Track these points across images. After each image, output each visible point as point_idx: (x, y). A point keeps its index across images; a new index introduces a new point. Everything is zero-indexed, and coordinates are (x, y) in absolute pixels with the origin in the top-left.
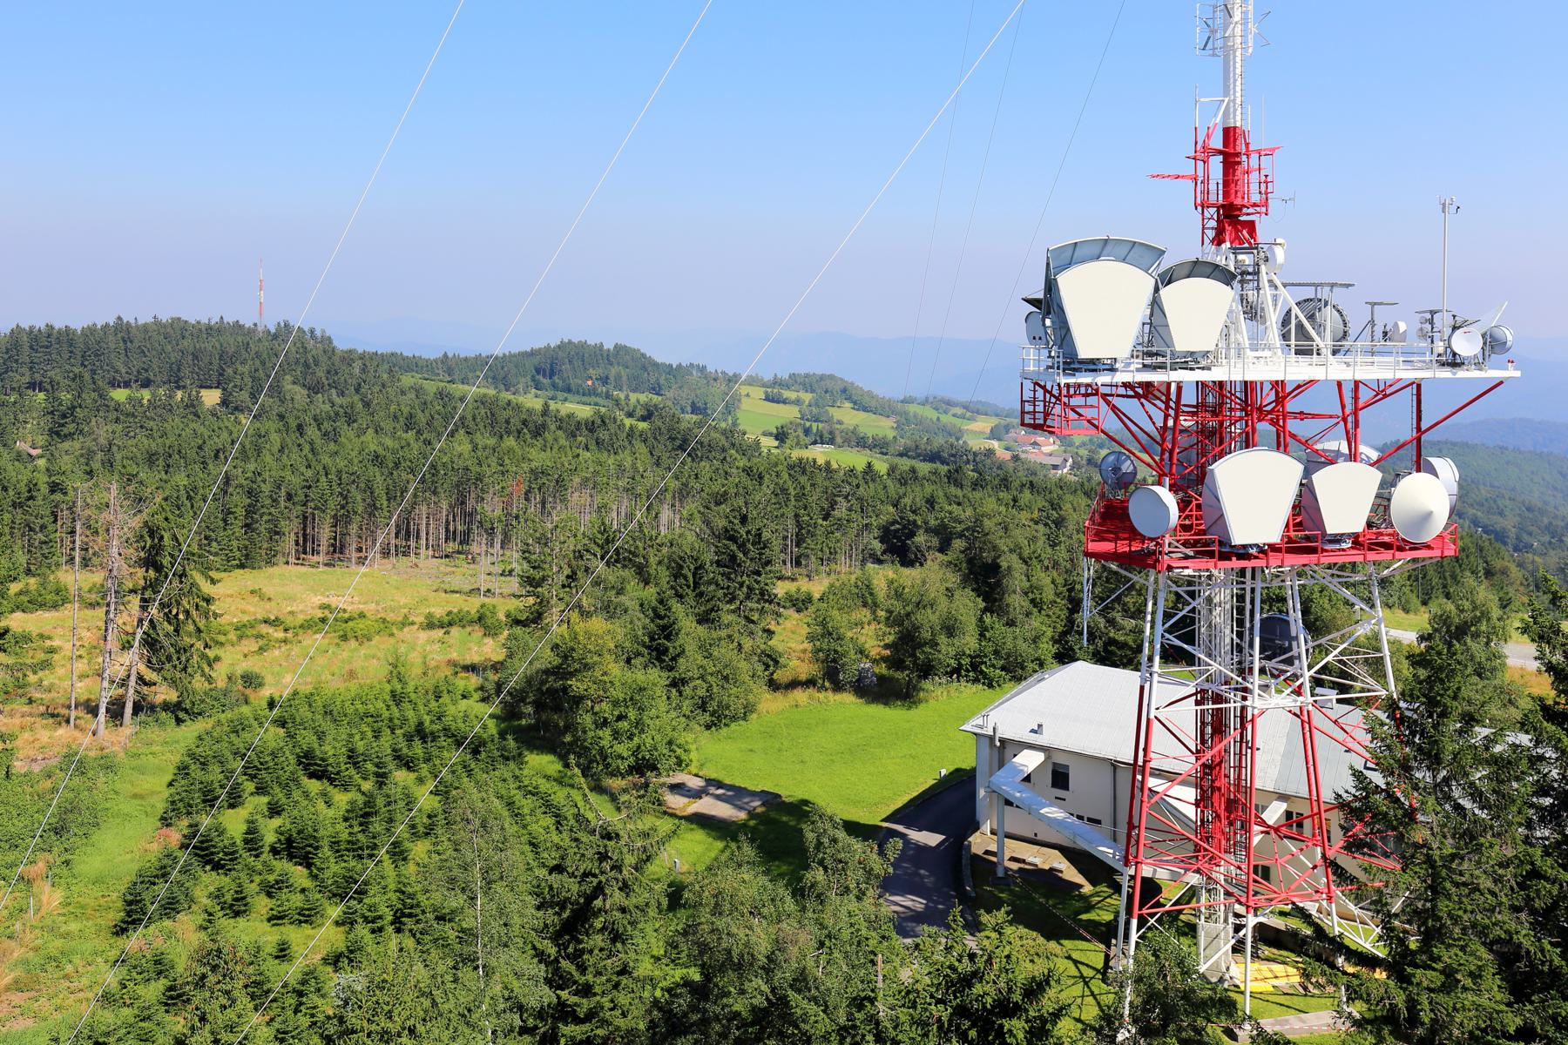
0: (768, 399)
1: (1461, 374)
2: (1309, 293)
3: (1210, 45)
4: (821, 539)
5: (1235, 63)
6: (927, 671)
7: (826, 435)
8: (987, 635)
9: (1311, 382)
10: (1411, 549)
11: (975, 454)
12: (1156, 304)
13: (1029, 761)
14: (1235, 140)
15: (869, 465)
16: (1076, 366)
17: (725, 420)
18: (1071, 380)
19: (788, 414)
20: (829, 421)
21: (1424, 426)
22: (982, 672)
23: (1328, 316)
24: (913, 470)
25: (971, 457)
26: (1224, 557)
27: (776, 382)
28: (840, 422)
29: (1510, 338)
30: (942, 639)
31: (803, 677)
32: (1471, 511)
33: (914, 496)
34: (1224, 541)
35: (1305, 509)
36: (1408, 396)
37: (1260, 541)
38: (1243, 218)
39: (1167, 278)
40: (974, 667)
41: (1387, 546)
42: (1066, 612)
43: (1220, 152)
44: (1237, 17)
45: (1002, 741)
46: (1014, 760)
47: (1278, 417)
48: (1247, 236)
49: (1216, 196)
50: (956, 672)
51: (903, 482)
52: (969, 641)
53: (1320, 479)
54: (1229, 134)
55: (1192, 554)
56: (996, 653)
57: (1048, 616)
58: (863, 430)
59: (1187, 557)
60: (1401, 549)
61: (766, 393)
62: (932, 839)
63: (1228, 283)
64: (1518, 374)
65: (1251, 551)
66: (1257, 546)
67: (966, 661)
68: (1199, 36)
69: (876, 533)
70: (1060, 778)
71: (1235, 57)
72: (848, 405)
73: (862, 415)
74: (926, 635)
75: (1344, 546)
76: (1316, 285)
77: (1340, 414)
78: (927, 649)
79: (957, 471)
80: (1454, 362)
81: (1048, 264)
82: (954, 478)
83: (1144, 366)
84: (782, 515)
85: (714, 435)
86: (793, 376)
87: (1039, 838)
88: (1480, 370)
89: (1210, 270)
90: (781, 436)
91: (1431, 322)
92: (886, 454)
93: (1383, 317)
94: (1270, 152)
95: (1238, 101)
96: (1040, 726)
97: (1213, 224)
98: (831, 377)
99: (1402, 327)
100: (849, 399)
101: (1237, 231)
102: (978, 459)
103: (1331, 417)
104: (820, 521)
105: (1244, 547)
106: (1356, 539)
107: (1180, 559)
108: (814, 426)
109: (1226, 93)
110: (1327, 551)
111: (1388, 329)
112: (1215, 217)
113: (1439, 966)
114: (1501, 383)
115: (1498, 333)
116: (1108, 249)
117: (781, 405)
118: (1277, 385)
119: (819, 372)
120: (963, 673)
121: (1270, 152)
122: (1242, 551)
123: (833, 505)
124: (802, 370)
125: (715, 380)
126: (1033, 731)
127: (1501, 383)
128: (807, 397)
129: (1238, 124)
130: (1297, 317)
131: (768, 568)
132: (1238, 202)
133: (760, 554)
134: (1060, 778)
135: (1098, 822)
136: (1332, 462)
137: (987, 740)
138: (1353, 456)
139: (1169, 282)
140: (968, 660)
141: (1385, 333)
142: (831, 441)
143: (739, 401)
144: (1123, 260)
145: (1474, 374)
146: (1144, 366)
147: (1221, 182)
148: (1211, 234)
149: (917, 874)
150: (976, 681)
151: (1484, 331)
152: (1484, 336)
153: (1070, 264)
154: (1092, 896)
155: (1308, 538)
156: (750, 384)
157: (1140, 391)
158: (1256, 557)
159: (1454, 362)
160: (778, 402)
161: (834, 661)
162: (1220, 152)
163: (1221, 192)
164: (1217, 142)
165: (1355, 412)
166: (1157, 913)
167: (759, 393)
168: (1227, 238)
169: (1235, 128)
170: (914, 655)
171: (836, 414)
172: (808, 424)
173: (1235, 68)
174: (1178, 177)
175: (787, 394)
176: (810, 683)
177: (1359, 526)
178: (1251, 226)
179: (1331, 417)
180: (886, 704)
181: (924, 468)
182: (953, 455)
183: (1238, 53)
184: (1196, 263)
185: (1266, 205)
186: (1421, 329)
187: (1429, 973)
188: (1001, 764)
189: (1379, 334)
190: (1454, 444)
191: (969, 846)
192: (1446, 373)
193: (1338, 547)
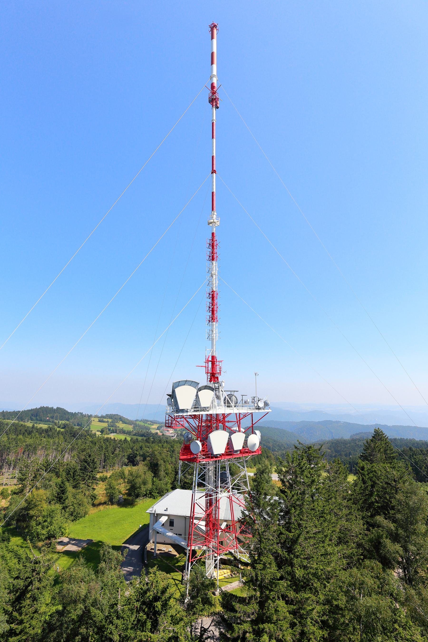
1: (260, 411)
2: (229, 393)
3: (209, 338)
7: (115, 431)
11: (153, 434)
12: (197, 396)
15: (126, 438)
16: (179, 411)
18: (178, 415)
19: (105, 425)
20: (116, 427)
22: (152, 495)
24: (137, 439)
27: (102, 417)
28: (119, 427)
30: (142, 486)
31: (103, 502)
32: (263, 442)
34: (212, 454)
35: (230, 444)
36: (250, 415)
37: (220, 453)
38: (216, 376)
39: (200, 390)
40: (150, 493)
41: (247, 452)
43: (211, 361)
44: (214, 332)
45: (157, 514)
47: (224, 422)
49: (210, 371)
51: (134, 443)
52: (149, 486)
53: (233, 437)
54: (213, 357)
55: (205, 457)
57: (170, 477)
58: (124, 429)
59: (203, 458)
60: (250, 453)
61: (99, 420)
62: (136, 547)
64: (271, 411)
66: (219, 454)
67: (148, 492)
72: (121, 422)
73: (125, 425)
74: (138, 485)
76: (231, 391)
78: (138, 489)
79: (148, 439)
80: (259, 408)
82: (147, 441)
90: (102, 431)
92: (130, 435)
94: (221, 361)
96: (167, 509)
97: (209, 377)
98: (117, 415)
99: (248, 401)
100: (122, 421)
103: (234, 422)
105: (216, 455)
107: (202, 459)
108: (111, 428)
115: (267, 402)
118: (223, 414)
120: (147, 495)
125: (85, 416)
126: (165, 510)
128: (110, 420)
132: (215, 372)
133: (93, 466)
135: (181, 535)
138: (239, 431)
139: (200, 391)
140: (149, 492)
141: (245, 402)
142: (116, 432)
144: (190, 385)
145: (263, 411)
146: (194, 411)
148: (209, 379)
150: (151, 497)
152: (264, 402)
153: (178, 386)
154: (179, 558)
155: (230, 452)
156: (94, 417)
158: (219, 457)
159: (259, 408)
162: (211, 361)
165: (240, 420)
167: (97, 420)
170: (134, 492)
171: (117, 424)
172: (110, 428)
175: (105, 420)
176: (105, 503)
178: (217, 378)
179: (234, 422)
180: (126, 507)
181: (140, 438)
182: (148, 435)
188: (156, 521)
189: (244, 402)
190: (259, 427)
192: (257, 411)
193: (237, 453)
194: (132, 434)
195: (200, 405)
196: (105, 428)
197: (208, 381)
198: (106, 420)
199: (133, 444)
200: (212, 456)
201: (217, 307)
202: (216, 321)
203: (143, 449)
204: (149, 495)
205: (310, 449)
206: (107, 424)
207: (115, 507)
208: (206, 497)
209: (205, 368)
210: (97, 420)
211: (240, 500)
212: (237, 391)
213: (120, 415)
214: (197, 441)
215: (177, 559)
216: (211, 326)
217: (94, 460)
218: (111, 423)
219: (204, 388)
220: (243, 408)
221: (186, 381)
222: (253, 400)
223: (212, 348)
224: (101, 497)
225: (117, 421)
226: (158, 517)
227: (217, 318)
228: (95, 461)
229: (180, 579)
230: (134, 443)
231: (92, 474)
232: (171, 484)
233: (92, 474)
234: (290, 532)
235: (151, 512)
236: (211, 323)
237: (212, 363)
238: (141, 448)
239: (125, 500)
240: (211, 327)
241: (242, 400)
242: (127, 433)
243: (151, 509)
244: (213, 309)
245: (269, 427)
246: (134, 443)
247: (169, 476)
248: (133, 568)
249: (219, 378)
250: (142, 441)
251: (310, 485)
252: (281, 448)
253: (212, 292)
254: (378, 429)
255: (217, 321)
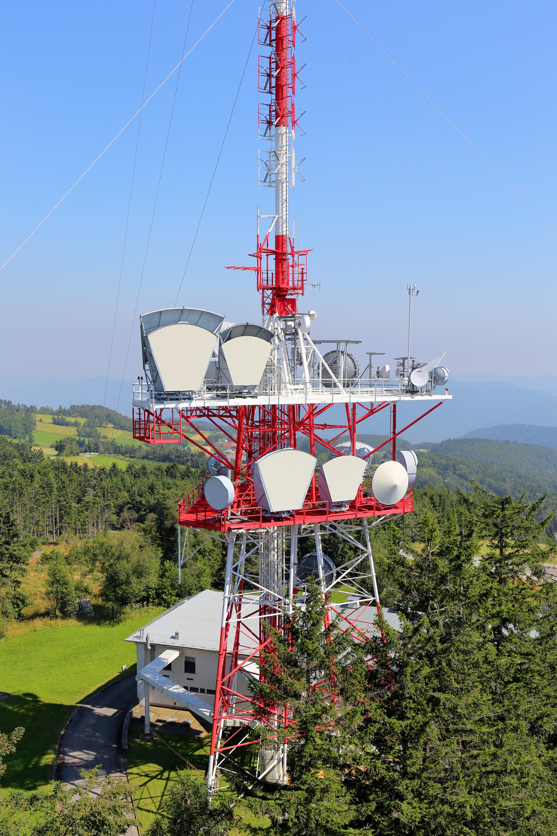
0: (56, 422)
1: (417, 398)
2: (333, 347)
3: (268, 180)
4: (74, 516)
5: (282, 191)
6: (124, 601)
7: (93, 446)
8: (167, 574)
9: (330, 405)
10: (385, 509)
11: (192, 455)
13: (170, 656)
14: (283, 244)
15: (114, 465)
16: (165, 396)
17: (24, 438)
18: (162, 406)
19: (70, 432)
20: (98, 436)
21: (397, 432)
22: (163, 599)
23: (342, 361)
24: (144, 468)
25: (189, 458)
26: (266, 520)
27: (61, 411)
28: (105, 437)
29: (447, 374)
30: (134, 579)
31: (43, 610)
32: (488, 480)
33: (142, 484)
34: (266, 511)
36: (388, 410)
37: (290, 509)
38: (288, 297)
39: (228, 336)
40: (158, 595)
41: (370, 508)
42: (221, 556)
43: (273, 252)
44: (283, 160)
45: (153, 646)
46: (160, 656)
47: (309, 428)
48: (290, 308)
50: (145, 600)
51: (136, 476)
52: (153, 580)
53: (327, 467)
54: (280, 240)
55: (246, 519)
56: (172, 586)
57: (209, 560)
58: (119, 442)
59: (243, 521)
60: (378, 509)
61: (54, 419)
62: (109, 712)
63: (268, 341)
64: (450, 397)
65: (283, 516)
66: (289, 512)
67: (152, 593)
68: (261, 173)
69: (113, 510)
70: (190, 666)
71: (282, 187)
72: (111, 425)
73: (120, 432)
74: (123, 577)
75: (344, 509)
76: (338, 342)
77: (348, 425)
78: (124, 587)
79: (172, 467)
80: (412, 390)
81: (141, 326)
82: (170, 473)
83: (217, 396)
84: (48, 502)
85: (8, 448)
86: (73, 407)
87: (178, 705)
88: (430, 395)
89: (256, 331)
90: (60, 448)
91: (403, 365)
92: (134, 457)
93: (377, 362)
94: (304, 253)
95: (284, 218)
96: (177, 634)
97: (269, 301)
98: (100, 407)
99: (388, 368)
100: (111, 421)
101: (285, 306)
102: (194, 459)
103: (341, 427)
104: (74, 504)
106: (352, 505)
107: (238, 523)
108: (87, 440)
109: (277, 212)
110: (332, 513)
111: (380, 370)
112: (271, 297)
113: (305, 787)
114: (441, 403)
115: (439, 371)
116: (185, 316)
117: (64, 427)
118: (312, 406)
119: (91, 404)
120: (151, 600)
121: (304, 253)
122: (278, 516)
123: (84, 493)
124: (79, 403)
125: (17, 410)
126: (173, 637)
127: (441, 403)
128: (82, 421)
129: (284, 234)
130: (323, 365)
131: (15, 539)
132: (284, 286)
133: (9, 530)
134: (190, 666)
136: (341, 455)
137: (143, 646)
139: (229, 339)
140: (154, 592)
141: (378, 372)
142: (96, 450)
143: (35, 424)
144: (196, 325)
145: (426, 398)
146: (217, 396)
147: (274, 272)
148: (267, 307)
149: (94, 735)
150: (159, 604)
151: (430, 370)
152: (431, 373)
153: (159, 326)
154: (206, 738)
155: (324, 506)
156: (42, 413)
157: (234, 413)
158: (287, 519)
159: (412, 390)
160: (62, 425)
161: (62, 598)
162: (273, 252)
163: (274, 279)
164: (272, 247)
165: (354, 425)
166: (241, 743)
167: (48, 419)
168: (277, 310)
169: (282, 236)
170: (114, 591)
171: (102, 431)
172: (82, 439)
173: (282, 195)
174: (246, 269)
175: (68, 419)
176: (47, 614)
177: (352, 496)
179: (341, 427)
180: (99, 624)
181: (151, 465)
182: (178, 457)
183: (284, 185)
184: (247, 326)
185: (302, 288)
186: (398, 370)
187: (300, 792)
188: (153, 658)
189: (374, 373)
190: (480, 440)
191: (132, 713)
192: (407, 398)
193: (339, 510)
194: (138, 454)
195: (230, 381)
196: (68, 439)
197: (266, 311)
198: (72, 420)
199: (133, 478)
200: (269, 515)
201: (294, 75)
202: (290, 124)
203: (155, 491)
204: (154, 599)
205: (507, 506)
206: (75, 429)
207: (73, 623)
208: (260, 615)
209: (254, 274)
210: (48, 419)
211: (351, 622)
212: (358, 342)
213: (107, 409)
214: (222, 478)
215: (200, 740)
216: (274, 139)
217: (8, 517)
218: (84, 426)
219: (241, 331)
220: (373, 389)
221: (182, 311)
222: (401, 368)
223: (277, 212)
224: (40, 601)
225: (101, 423)
226: (156, 652)
227: (293, 112)
228: (12, 519)
229: (142, 797)
230: (135, 476)
231: (7, 549)
232: (213, 575)
233: (7, 549)
234: (402, 717)
235: (138, 640)
236: (273, 127)
237: (276, 259)
238: (152, 488)
239: (97, 608)
240: (274, 143)
241: (370, 366)
242: (126, 453)
243: (138, 634)
244: (278, 78)
245: (507, 442)
246: (136, 476)
247: (206, 557)
248: (95, 754)
249: (297, 302)
250: (157, 472)
251: (476, 604)
252: (535, 495)
253: (277, 18)
254: (57, 442)
255: (294, 122)
